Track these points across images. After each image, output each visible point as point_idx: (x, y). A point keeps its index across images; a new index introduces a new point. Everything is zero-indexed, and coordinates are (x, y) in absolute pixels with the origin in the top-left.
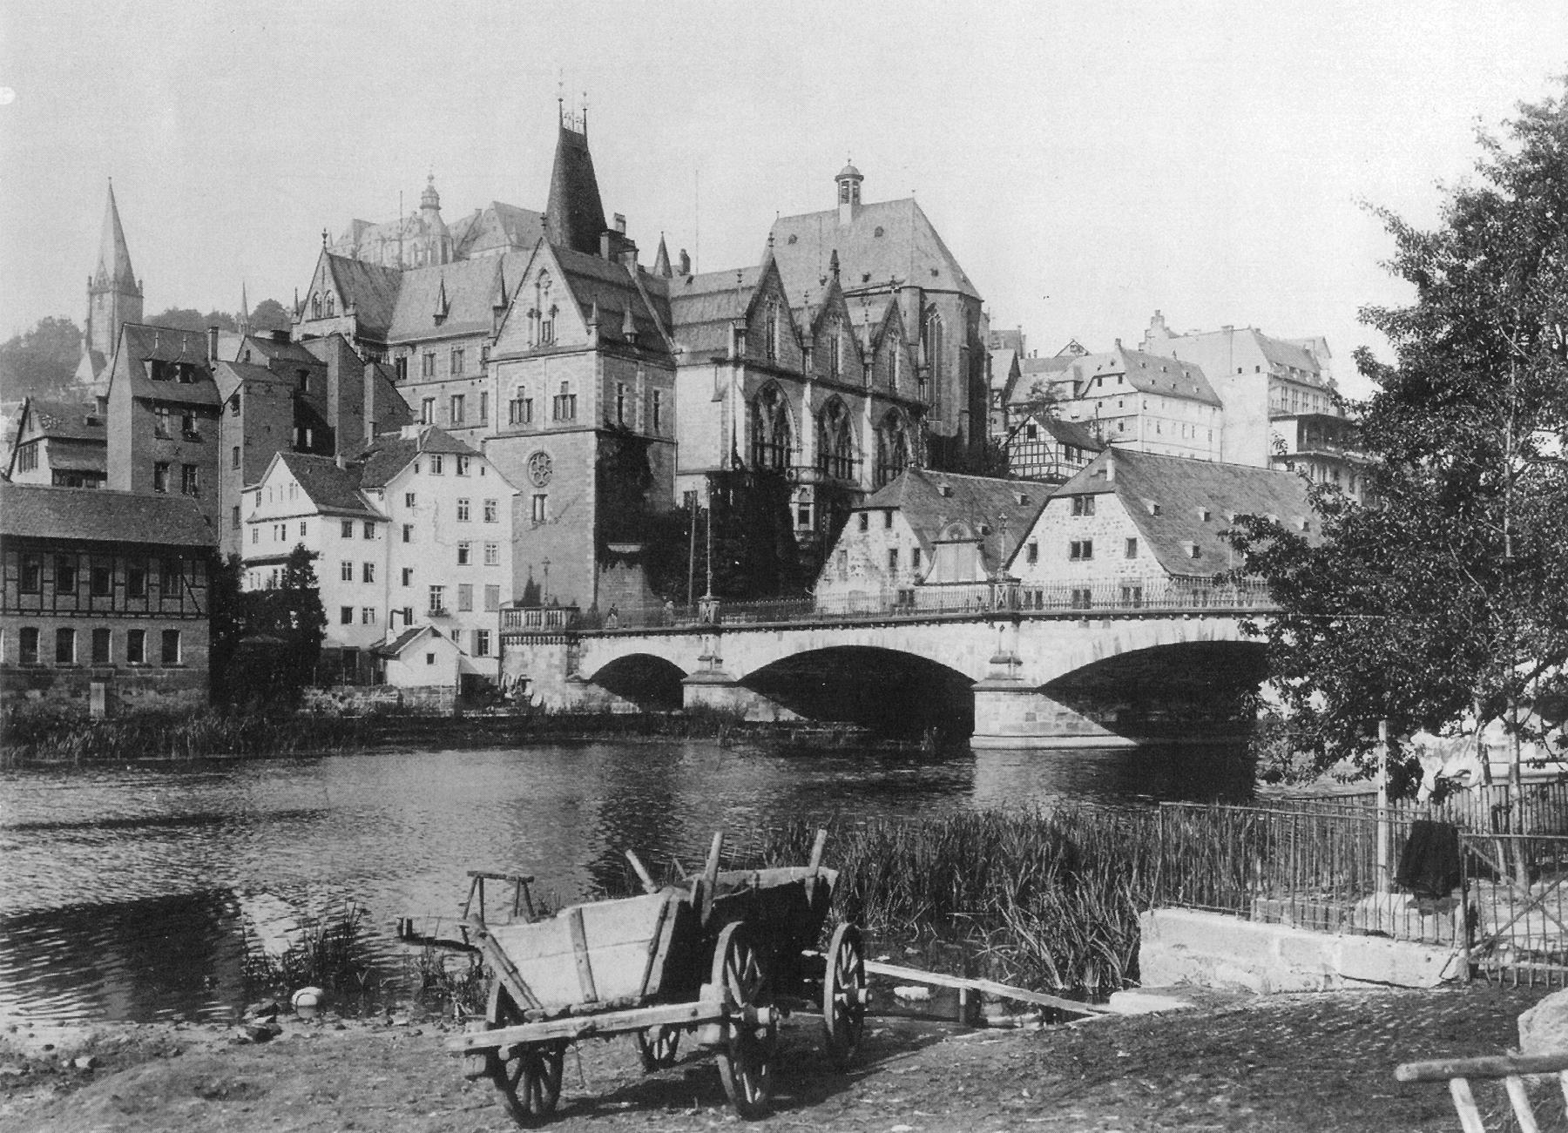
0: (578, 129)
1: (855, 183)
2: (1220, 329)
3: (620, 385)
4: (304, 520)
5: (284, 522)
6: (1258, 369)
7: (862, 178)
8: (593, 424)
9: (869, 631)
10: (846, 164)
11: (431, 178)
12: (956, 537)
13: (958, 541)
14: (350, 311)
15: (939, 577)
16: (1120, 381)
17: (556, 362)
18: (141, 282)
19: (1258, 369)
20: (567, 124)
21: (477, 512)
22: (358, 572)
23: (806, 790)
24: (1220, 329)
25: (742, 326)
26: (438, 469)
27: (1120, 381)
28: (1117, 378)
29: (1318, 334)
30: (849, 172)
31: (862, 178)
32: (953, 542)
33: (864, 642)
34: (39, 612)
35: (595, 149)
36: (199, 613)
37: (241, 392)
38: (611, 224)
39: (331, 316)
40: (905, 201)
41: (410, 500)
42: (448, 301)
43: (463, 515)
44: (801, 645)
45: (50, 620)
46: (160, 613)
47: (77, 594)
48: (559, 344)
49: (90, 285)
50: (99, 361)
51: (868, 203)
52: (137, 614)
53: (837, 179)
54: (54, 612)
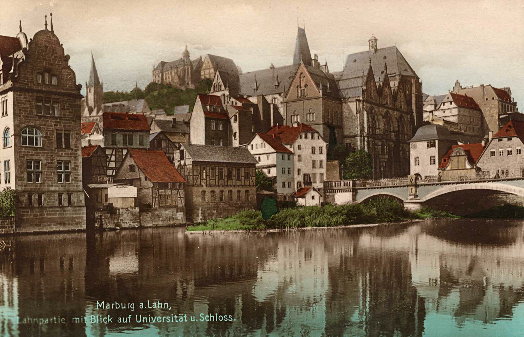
0: (302, 27)
1: (376, 42)
2: (479, 86)
3: (328, 109)
4: (268, 155)
5: (259, 156)
6: (493, 99)
7: (377, 40)
8: (322, 122)
9: (455, 185)
10: (372, 36)
11: (186, 47)
12: (458, 154)
13: (459, 156)
14: (227, 88)
15: (451, 168)
16: (451, 104)
17: (307, 102)
18: (102, 83)
19: (493, 99)
20: (300, 26)
21: (317, 151)
22: (286, 170)
23: (178, 248)
24: (479, 86)
25: (364, 88)
26: (306, 137)
27: (451, 104)
28: (450, 103)
29: (506, 86)
30: (374, 38)
31: (377, 40)
32: (457, 156)
33: (479, 188)
34: (215, 185)
35: (306, 32)
36: (254, 185)
37: (237, 115)
38: (313, 58)
39: (221, 91)
40: (394, 47)
41: (299, 147)
42: (258, 85)
43: (313, 152)
44: (493, 188)
45: (217, 188)
46: (244, 185)
47: (224, 180)
48: (308, 97)
49: (86, 85)
50: (91, 110)
51: (380, 48)
52: (239, 185)
53: (369, 41)
54: (219, 186)
